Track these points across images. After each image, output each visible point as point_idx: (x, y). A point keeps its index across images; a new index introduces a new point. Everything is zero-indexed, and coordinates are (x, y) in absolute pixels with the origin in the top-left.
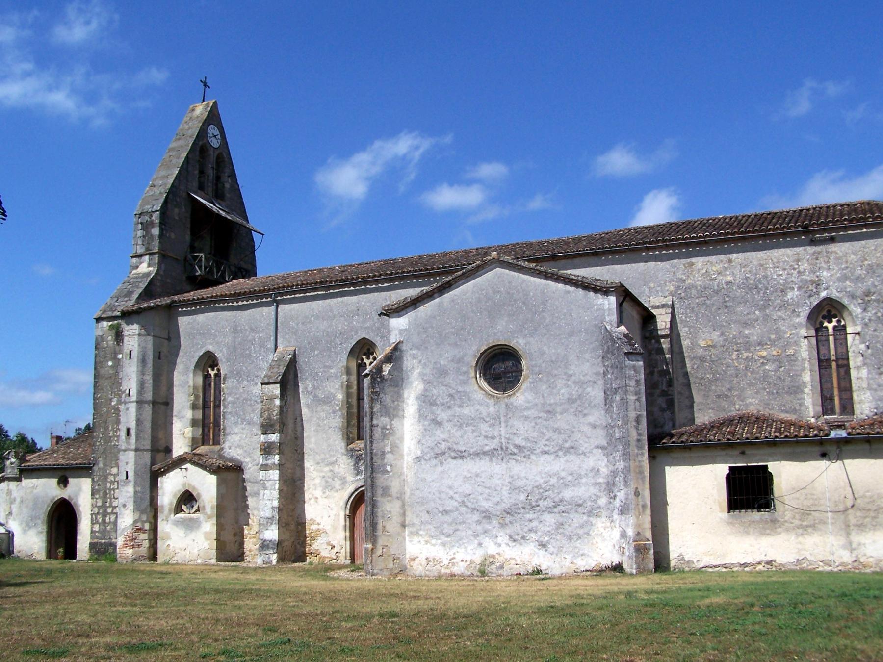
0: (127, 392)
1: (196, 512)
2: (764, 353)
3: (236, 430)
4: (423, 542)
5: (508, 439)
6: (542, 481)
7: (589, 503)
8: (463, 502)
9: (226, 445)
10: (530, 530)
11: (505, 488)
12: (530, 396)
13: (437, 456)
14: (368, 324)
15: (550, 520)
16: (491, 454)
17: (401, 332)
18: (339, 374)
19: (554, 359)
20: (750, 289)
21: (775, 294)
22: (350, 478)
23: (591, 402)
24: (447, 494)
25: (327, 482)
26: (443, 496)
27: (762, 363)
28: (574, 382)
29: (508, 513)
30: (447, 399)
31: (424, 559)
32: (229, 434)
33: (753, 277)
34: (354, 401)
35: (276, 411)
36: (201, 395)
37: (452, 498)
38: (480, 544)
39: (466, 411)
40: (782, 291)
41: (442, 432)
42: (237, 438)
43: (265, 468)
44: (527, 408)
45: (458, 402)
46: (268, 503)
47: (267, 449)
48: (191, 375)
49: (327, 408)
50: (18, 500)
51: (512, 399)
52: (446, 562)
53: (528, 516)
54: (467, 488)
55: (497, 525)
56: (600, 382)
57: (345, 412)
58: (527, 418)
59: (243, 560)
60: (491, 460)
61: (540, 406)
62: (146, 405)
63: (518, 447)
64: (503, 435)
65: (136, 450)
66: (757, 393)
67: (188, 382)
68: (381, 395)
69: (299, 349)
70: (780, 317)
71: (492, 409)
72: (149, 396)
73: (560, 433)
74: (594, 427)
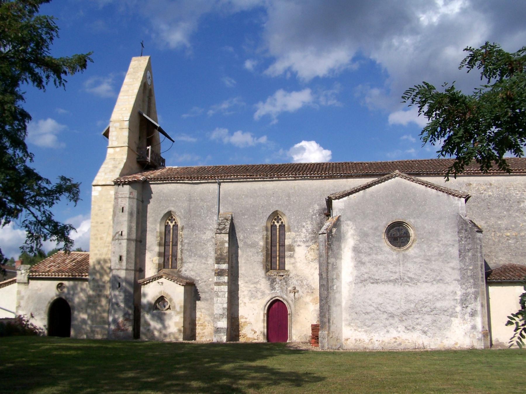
0: (120, 233)
1: (168, 309)
2: (508, 234)
3: (191, 260)
4: (353, 330)
5: (404, 274)
6: (424, 297)
7: (451, 310)
8: (378, 307)
9: (183, 269)
10: (417, 324)
11: (402, 301)
12: (417, 250)
13: (362, 281)
14: (280, 202)
15: (429, 318)
16: (394, 281)
17: (340, 210)
18: (261, 230)
19: (430, 231)
20: (501, 200)
21: (514, 204)
22: (268, 292)
23: (451, 256)
24: (368, 303)
25: (252, 294)
26: (366, 304)
27: (508, 239)
28: (442, 244)
29: (404, 314)
30: (368, 250)
31: (353, 340)
32: (185, 262)
33: (503, 194)
34: (269, 247)
35: (226, 250)
36: (164, 237)
37: (371, 305)
38: (388, 332)
39: (379, 257)
40: (518, 202)
41: (365, 268)
42: (191, 265)
43: (218, 284)
44: (415, 257)
45: (375, 252)
46: (220, 305)
47: (220, 273)
48: (158, 225)
49: (253, 250)
50: (26, 297)
51: (407, 252)
52: (367, 341)
53: (416, 316)
54: (380, 300)
55: (398, 321)
56: (457, 245)
57: (265, 252)
58: (415, 262)
59: (195, 339)
60: (394, 285)
61: (422, 256)
62: (132, 242)
63: (409, 278)
64: (401, 271)
65: (127, 269)
66: (505, 254)
67: (156, 229)
68: (332, 246)
69: (234, 213)
70: (517, 216)
71: (395, 257)
72: (134, 236)
73: (434, 272)
74: (453, 269)
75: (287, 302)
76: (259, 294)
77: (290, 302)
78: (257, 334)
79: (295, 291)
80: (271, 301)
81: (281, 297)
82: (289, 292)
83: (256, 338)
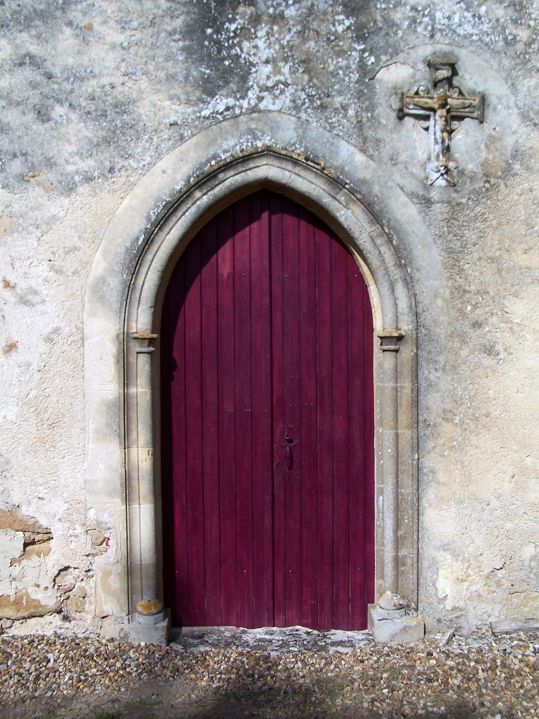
22: (160, 104)
75: (375, 214)
76: (71, 137)
77: (404, 210)
78: (56, 555)
79: (445, 98)
80: (203, 199)
81: (309, 162)
82: (386, 113)
83: (48, 599)
